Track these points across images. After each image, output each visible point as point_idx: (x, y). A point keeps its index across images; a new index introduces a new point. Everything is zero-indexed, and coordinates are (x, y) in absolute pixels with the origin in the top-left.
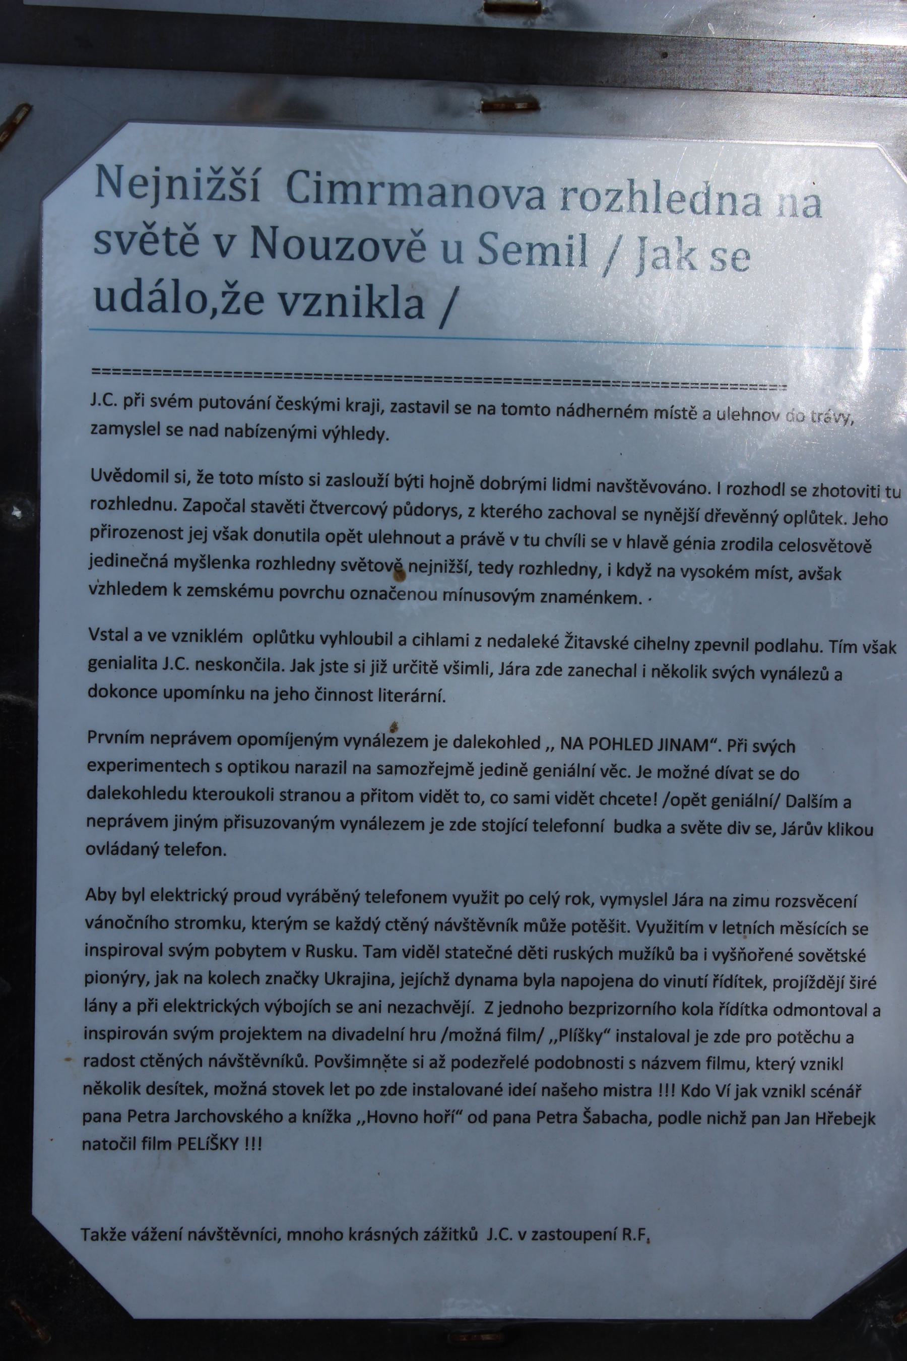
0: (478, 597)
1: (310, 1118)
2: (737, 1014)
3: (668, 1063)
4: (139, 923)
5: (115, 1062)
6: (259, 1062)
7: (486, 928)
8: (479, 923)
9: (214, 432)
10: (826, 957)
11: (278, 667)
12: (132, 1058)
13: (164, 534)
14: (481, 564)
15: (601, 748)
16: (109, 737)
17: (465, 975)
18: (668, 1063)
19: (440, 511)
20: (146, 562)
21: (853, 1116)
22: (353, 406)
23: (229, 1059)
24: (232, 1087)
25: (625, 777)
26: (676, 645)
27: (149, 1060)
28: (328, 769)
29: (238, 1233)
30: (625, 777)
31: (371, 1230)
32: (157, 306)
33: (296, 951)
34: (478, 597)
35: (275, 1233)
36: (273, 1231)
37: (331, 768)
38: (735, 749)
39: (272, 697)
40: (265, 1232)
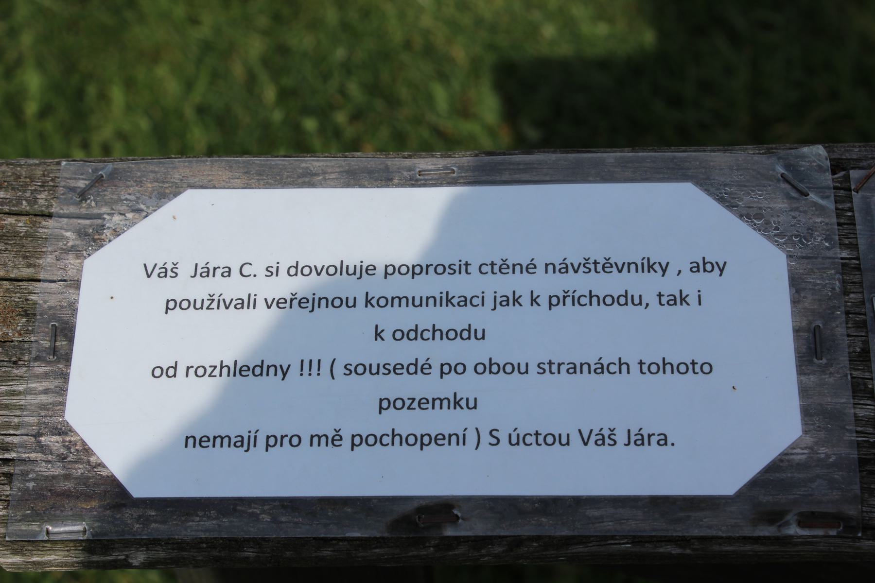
5: (411, 440)
7: (614, 269)
11: (666, 439)
15: (427, 445)
26: (272, 370)
27: (534, 437)
32: (239, 444)
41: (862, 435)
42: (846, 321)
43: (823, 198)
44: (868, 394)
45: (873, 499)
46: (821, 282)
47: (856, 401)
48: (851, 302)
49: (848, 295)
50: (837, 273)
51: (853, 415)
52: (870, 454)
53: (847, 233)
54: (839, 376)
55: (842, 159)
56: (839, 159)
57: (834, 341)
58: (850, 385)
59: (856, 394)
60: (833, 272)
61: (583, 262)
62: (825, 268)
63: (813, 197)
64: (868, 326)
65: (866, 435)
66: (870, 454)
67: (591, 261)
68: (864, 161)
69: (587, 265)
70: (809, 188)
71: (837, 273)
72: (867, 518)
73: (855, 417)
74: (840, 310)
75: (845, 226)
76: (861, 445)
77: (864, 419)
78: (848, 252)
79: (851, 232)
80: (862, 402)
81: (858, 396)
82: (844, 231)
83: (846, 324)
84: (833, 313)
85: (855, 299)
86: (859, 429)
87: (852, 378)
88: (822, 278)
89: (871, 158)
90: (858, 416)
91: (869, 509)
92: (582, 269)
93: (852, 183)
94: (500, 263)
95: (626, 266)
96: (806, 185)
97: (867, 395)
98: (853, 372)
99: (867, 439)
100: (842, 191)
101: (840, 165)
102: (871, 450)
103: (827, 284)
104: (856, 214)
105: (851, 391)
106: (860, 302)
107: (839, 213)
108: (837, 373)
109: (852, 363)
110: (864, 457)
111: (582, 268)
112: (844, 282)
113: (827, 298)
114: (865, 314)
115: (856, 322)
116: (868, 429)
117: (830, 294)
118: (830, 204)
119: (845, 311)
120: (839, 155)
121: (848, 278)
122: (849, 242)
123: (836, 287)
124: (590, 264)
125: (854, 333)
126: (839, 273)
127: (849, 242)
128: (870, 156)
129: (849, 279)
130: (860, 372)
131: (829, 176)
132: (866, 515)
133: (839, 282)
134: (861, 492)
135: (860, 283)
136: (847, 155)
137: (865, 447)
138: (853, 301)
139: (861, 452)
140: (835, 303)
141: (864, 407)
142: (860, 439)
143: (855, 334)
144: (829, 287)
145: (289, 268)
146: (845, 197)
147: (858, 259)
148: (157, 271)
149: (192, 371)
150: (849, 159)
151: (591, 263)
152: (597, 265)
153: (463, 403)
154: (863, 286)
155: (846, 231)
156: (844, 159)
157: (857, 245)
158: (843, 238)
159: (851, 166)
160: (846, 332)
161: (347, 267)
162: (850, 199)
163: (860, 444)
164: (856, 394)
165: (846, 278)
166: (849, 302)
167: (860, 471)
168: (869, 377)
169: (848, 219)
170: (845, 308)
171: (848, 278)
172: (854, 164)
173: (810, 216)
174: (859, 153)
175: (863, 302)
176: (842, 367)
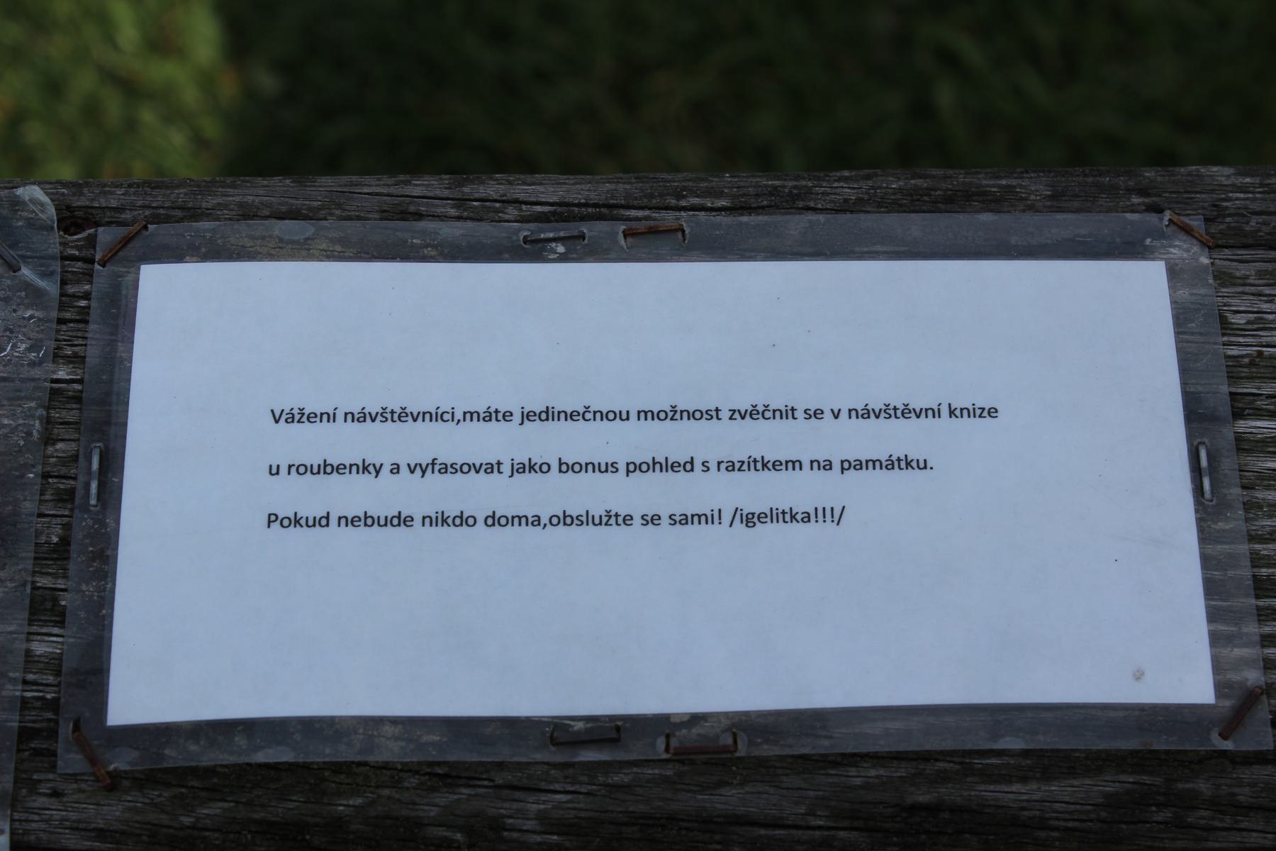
0: (603, 468)
1: (958, 413)
2: (547, 419)
3: (737, 413)
4: (778, 414)
6: (910, 412)
7: (410, 418)
10: (751, 415)
12: (717, 410)
13: (698, 415)
16: (743, 413)
18: (737, 413)
20: (588, 416)
23: (370, 413)
28: (733, 465)
29: (909, 410)
33: (836, 413)
34: (603, 468)
35: (453, 413)
36: (451, 411)
37: (737, 465)
39: (517, 417)
40: (440, 412)
41: (34, 688)
42: (41, 490)
43: (43, 275)
44: (57, 616)
45: (34, 798)
46: (11, 422)
47: (34, 629)
48: (57, 457)
49: (54, 444)
50: (40, 406)
51: (23, 653)
52: (41, 721)
54: (13, 585)
55: (93, 207)
56: (87, 207)
57: (15, 525)
58: (27, 602)
59: (36, 617)
60: (33, 404)
61: (381, 411)
62: (20, 398)
63: (26, 272)
64: (76, 499)
65: (41, 688)
66: (41, 721)
67: (389, 410)
68: (128, 212)
69: (384, 415)
70: (23, 257)
71: (40, 406)
72: (21, 831)
73: (26, 656)
74: (34, 470)
75: (72, 325)
76: (30, 705)
77: (42, 659)
78: (69, 370)
79: (79, 335)
80: (44, 630)
81: (40, 620)
82: (68, 333)
83: (41, 495)
84: (22, 476)
85: (63, 452)
86: (31, 677)
87: (35, 588)
88: (13, 416)
89: (139, 206)
90: (33, 654)
91: (24, 816)
92: (379, 418)
93: (98, 249)
94: (399, 411)
95: (421, 415)
96: (20, 253)
97: (54, 618)
98: (38, 579)
99: (41, 694)
100: (80, 264)
101: (90, 217)
102: (44, 714)
103: (20, 425)
104: (94, 304)
105: (28, 612)
106: (71, 456)
107: (65, 300)
108: (10, 580)
109: (39, 562)
110: (30, 725)
111: (379, 417)
112: (48, 422)
113: (16, 449)
114: (75, 479)
115: (58, 492)
116: (45, 677)
117: (22, 443)
118: (51, 288)
119: (42, 473)
120: (88, 200)
121: (57, 415)
122: (74, 352)
123: (34, 431)
124: (386, 413)
125: (51, 510)
126: (44, 407)
127: (74, 352)
128: (140, 203)
129: (58, 417)
130: (50, 578)
131: (56, 237)
132: (18, 827)
133: (41, 422)
134: (14, 787)
135: (76, 423)
136: (102, 200)
137: (34, 708)
138: (60, 455)
139: (27, 718)
140: (28, 458)
141: (47, 638)
142: (29, 694)
143: (51, 512)
144: (22, 431)
146: (83, 273)
147: (80, 381)
148: (284, 417)
150: (104, 208)
153: (303, 522)
154: (79, 429)
155: (70, 334)
156: (96, 207)
157: (84, 357)
158: (65, 345)
159: (106, 219)
160: (37, 509)
162: (89, 276)
163: (28, 703)
164: (36, 617)
165: (55, 414)
166: (53, 457)
167: (19, 751)
168: (63, 587)
169: (79, 313)
170: (43, 468)
171: (57, 415)
172: (111, 217)
173: (15, 307)
174: (122, 197)
175: (75, 458)
176: (21, 570)
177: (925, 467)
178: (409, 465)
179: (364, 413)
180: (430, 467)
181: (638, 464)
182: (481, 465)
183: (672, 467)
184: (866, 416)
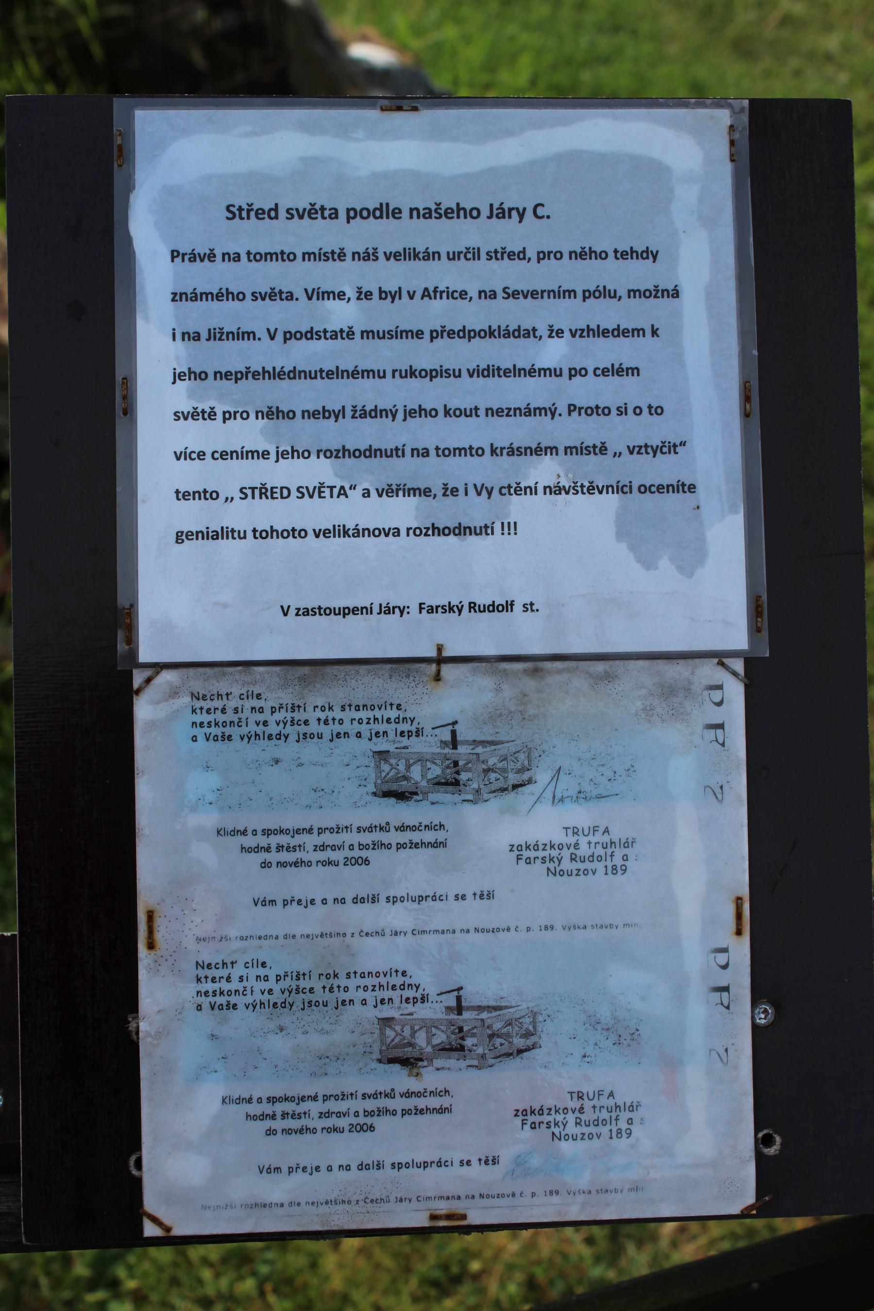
0: (381, 335)
8: (340, 253)
9: (587, 294)
14: (177, 492)
15: (354, 858)
17: (650, 249)
19: (397, 610)
21: (286, 411)
22: (498, 451)
24: (601, 252)
25: (542, 217)
30: (542, 217)
31: (428, 251)
34: (381, 335)
38: (179, 259)
53: (368, 1114)
69: (576, 488)
124: (577, 487)
145: (623, 858)
149: (411, 532)
151: (328, 210)
152: (446, 654)
161: (609, 291)
177: (615, 297)
178: (395, 827)
179: (559, 487)
180: (342, 847)
181: (648, 486)
182: (390, 529)
183: (279, 375)
184: (557, 492)
